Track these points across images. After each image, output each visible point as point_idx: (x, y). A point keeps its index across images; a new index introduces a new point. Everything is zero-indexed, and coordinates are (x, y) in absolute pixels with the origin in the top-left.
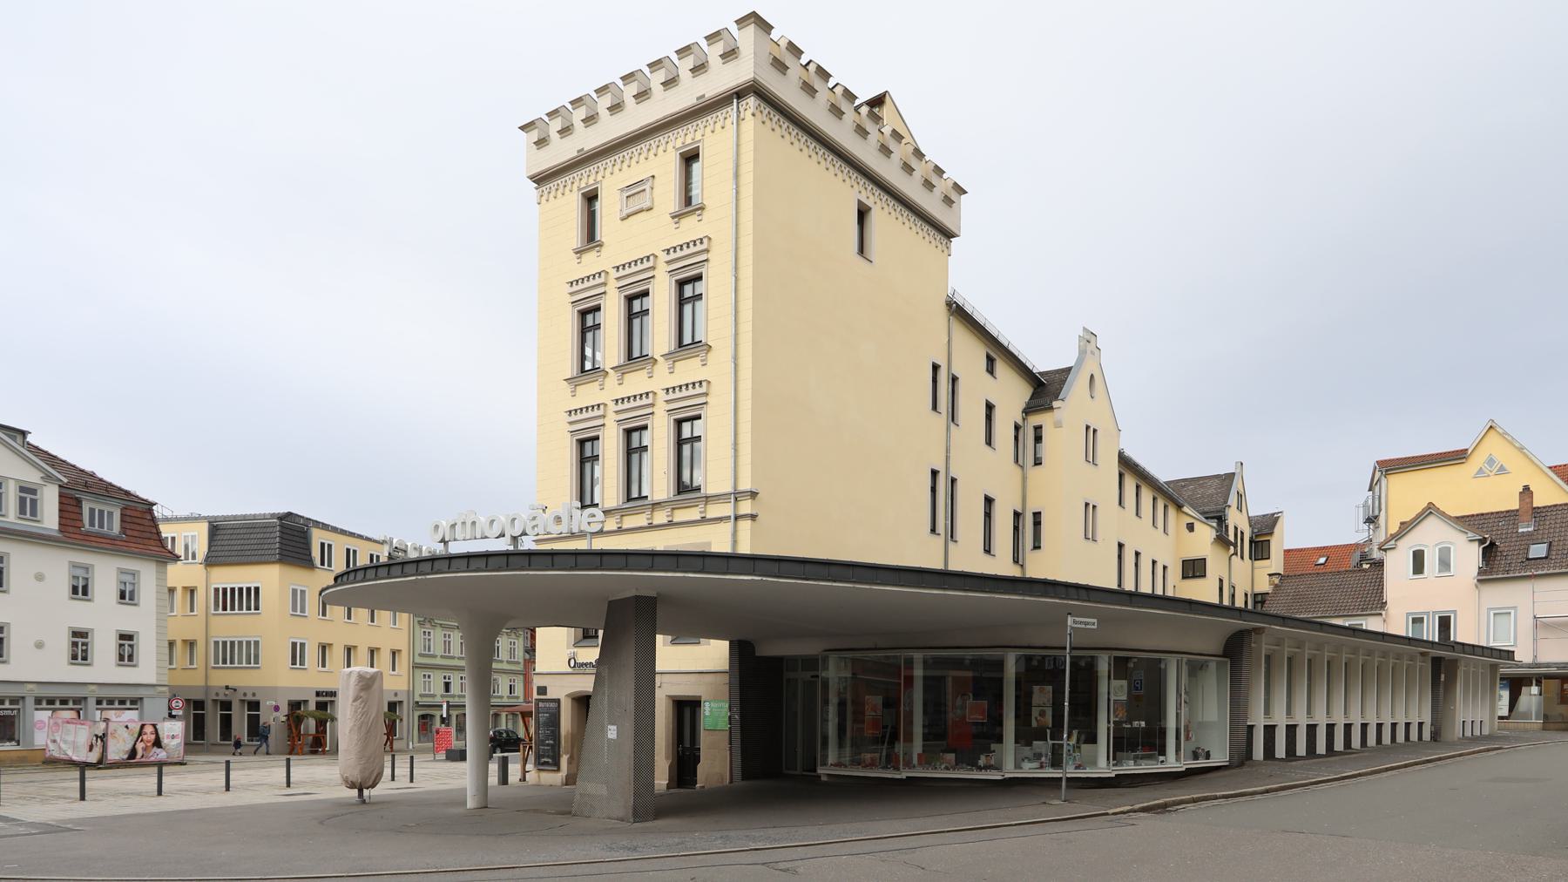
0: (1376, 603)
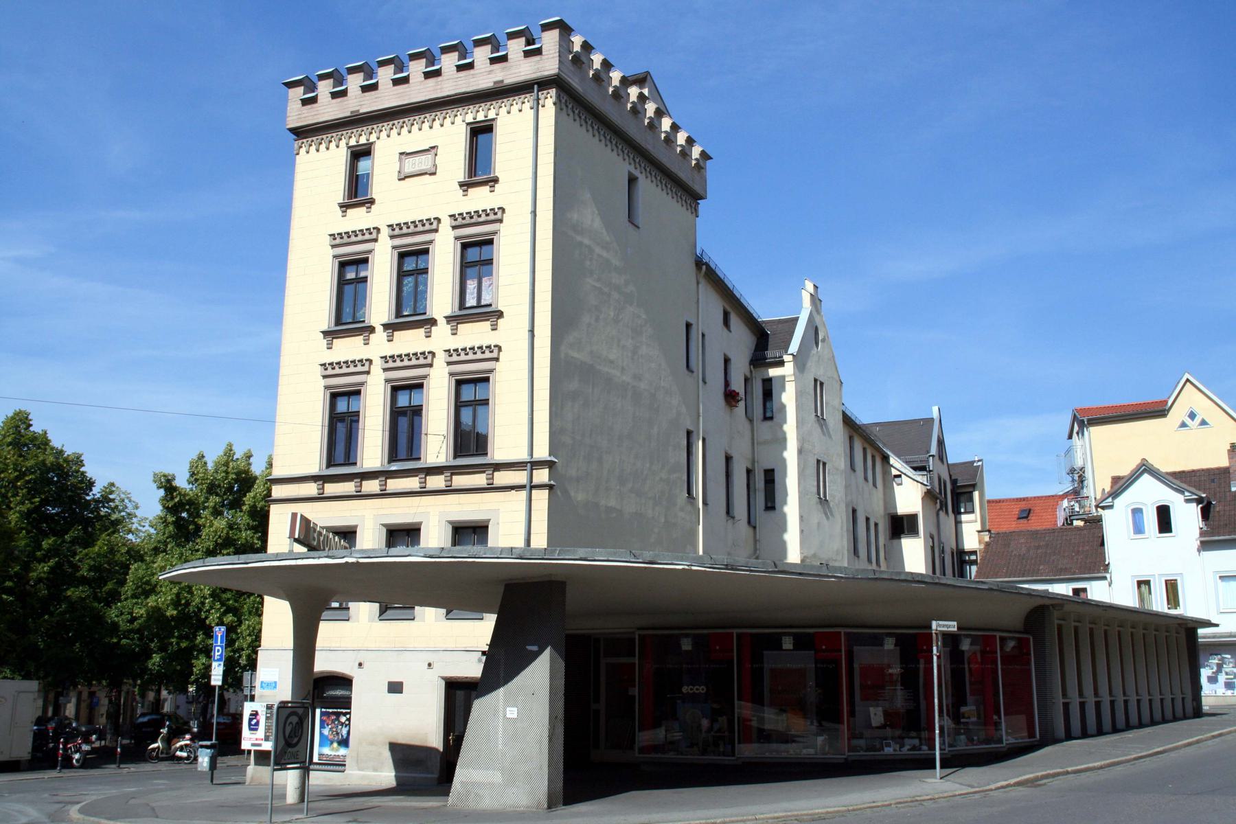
0: (1096, 565)
